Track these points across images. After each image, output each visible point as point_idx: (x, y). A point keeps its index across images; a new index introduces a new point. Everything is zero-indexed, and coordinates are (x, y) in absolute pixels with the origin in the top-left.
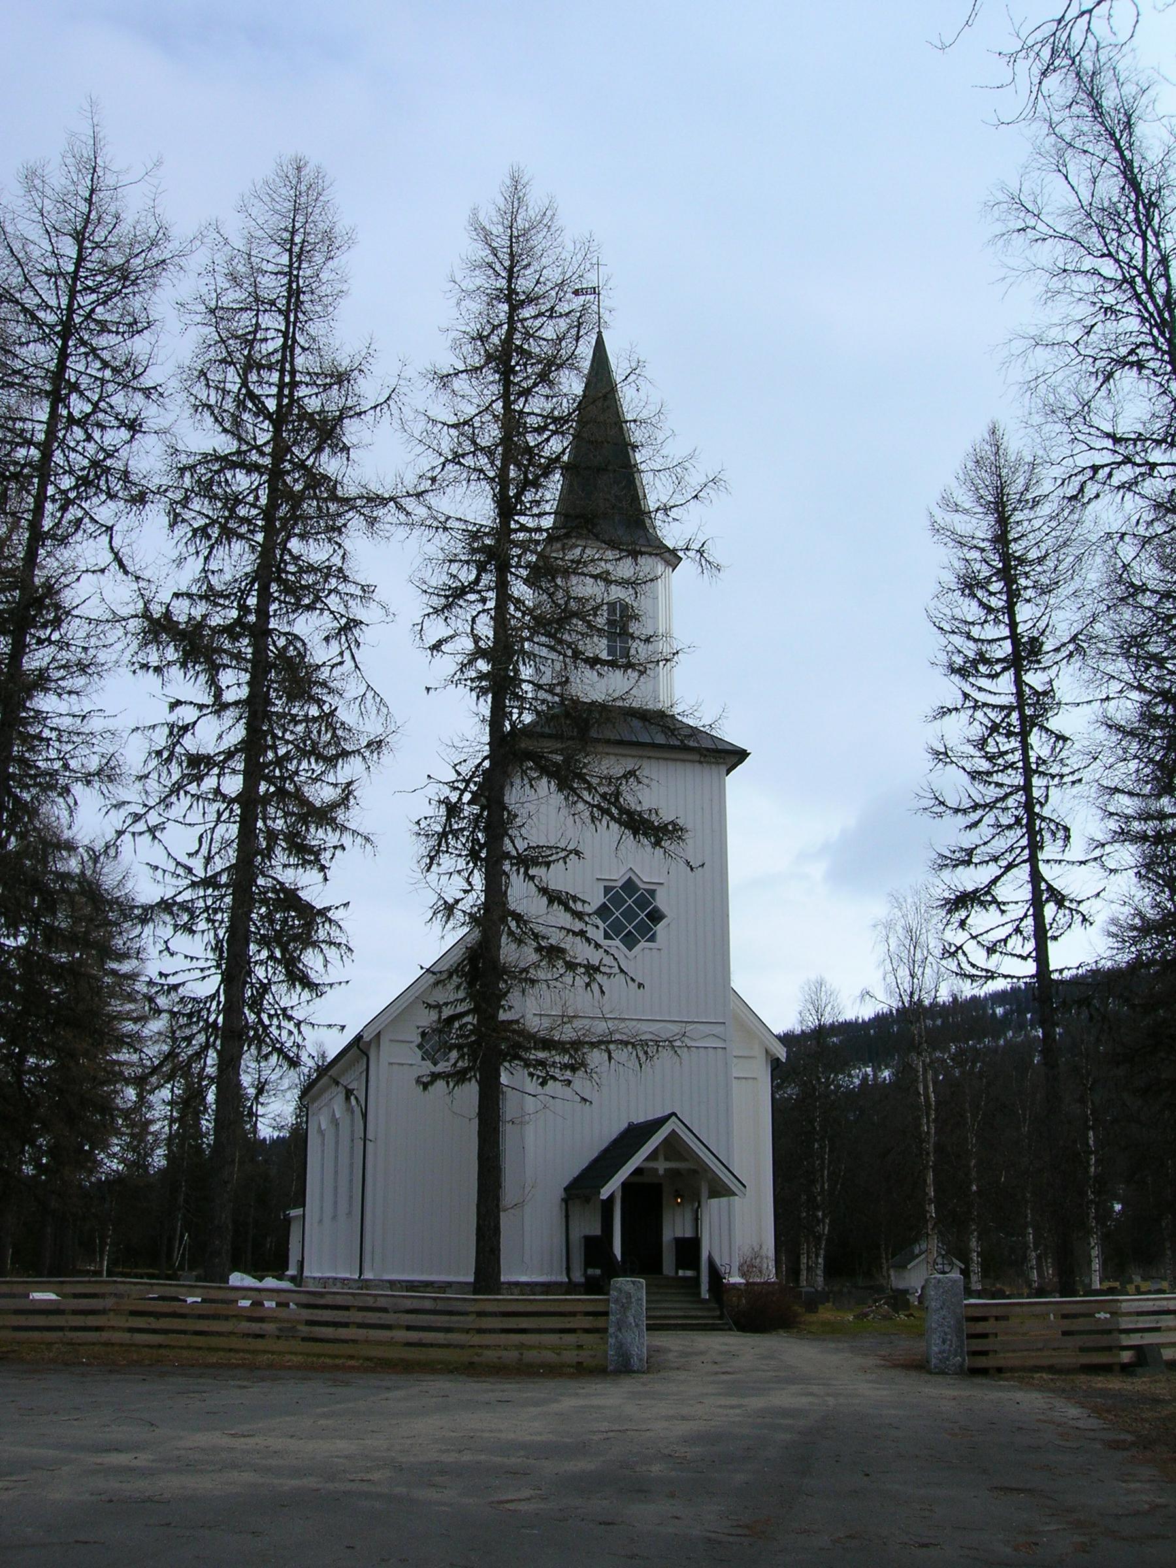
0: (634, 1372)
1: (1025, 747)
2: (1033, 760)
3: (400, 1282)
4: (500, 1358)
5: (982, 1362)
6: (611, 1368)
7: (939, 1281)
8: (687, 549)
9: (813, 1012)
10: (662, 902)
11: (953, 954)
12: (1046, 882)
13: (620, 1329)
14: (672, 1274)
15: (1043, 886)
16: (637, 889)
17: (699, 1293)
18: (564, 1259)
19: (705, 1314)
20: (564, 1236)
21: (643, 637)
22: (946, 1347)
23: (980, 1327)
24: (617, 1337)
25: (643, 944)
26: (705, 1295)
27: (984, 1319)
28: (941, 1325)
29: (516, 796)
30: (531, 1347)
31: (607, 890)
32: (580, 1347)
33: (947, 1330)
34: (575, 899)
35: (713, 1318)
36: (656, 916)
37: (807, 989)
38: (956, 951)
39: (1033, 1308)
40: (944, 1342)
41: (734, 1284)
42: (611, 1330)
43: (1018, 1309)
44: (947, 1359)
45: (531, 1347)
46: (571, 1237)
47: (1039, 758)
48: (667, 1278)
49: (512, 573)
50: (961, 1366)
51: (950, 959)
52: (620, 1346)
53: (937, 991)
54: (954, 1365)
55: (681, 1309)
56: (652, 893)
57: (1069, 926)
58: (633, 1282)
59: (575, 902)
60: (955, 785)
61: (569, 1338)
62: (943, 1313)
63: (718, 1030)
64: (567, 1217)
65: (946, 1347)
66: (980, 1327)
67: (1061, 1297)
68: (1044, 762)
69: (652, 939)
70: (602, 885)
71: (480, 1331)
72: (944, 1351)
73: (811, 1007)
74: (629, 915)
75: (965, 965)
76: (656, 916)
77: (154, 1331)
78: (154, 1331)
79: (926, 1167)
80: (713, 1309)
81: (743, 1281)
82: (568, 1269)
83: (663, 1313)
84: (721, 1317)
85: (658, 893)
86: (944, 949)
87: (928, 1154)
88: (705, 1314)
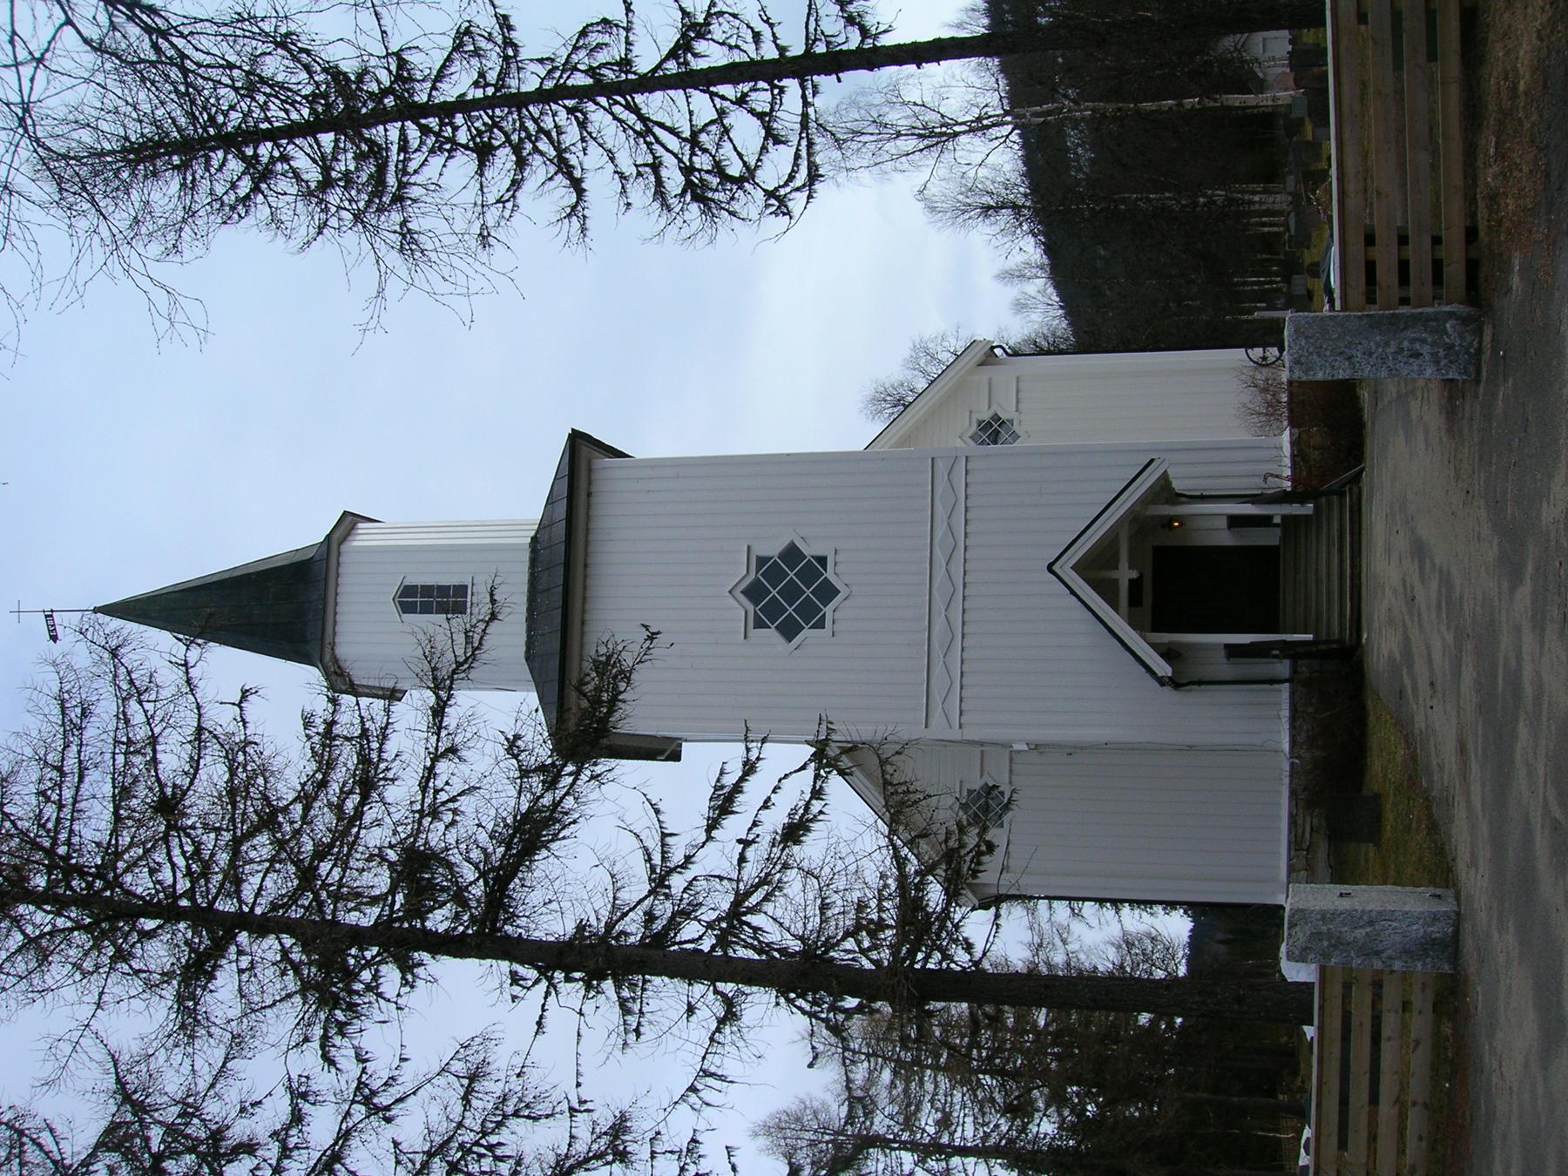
0: (1457, 933)
1: (463, 105)
2: (479, 94)
3: (1290, 859)
4: (1420, 1138)
5: (1455, 272)
6: (1447, 968)
8: (186, 664)
9: (967, 216)
10: (773, 549)
11: (782, 201)
13: (1377, 953)
14: (1278, 531)
15: (672, 66)
16: (757, 581)
17: (1306, 516)
18: (1255, 687)
21: (331, 708)
23: (1387, 275)
24: (1390, 958)
25: (829, 575)
26: (1308, 509)
27: (1370, 267)
28: (1384, 359)
29: (553, 926)
30: (1403, 1087)
31: (759, 624)
32: (1406, 1006)
33: (1392, 349)
35: (1342, 506)
36: (792, 554)
40: (1418, 355)
41: (1292, 444)
42: (1378, 965)
44: (1450, 347)
45: (1403, 1087)
46: (1228, 678)
47: (476, 84)
48: (1284, 538)
49: (252, 909)
50: (1464, 320)
56: (762, 561)
57: (735, 16)
58: (1292, 926)
59: (722, 787)
60: (543, 196)
63: (940, 464)
64: (1200, 683)
66: (1387, 275)
67: (1324, 25)
68: (482, 75)
69: (822, 560)
70: (753, 632)
71: (1373, 1138)
72: (1434, 355)
73: (960, 220)
75: (798, 182)
76: (792, 554)
79: (1138, 112)
80: (1329, 504)
81: (1287, 432)
82: (1272, 681)
83: (1335, 578)
84: (1341, 495)
85: (763, 554)
87: (1119, 109)
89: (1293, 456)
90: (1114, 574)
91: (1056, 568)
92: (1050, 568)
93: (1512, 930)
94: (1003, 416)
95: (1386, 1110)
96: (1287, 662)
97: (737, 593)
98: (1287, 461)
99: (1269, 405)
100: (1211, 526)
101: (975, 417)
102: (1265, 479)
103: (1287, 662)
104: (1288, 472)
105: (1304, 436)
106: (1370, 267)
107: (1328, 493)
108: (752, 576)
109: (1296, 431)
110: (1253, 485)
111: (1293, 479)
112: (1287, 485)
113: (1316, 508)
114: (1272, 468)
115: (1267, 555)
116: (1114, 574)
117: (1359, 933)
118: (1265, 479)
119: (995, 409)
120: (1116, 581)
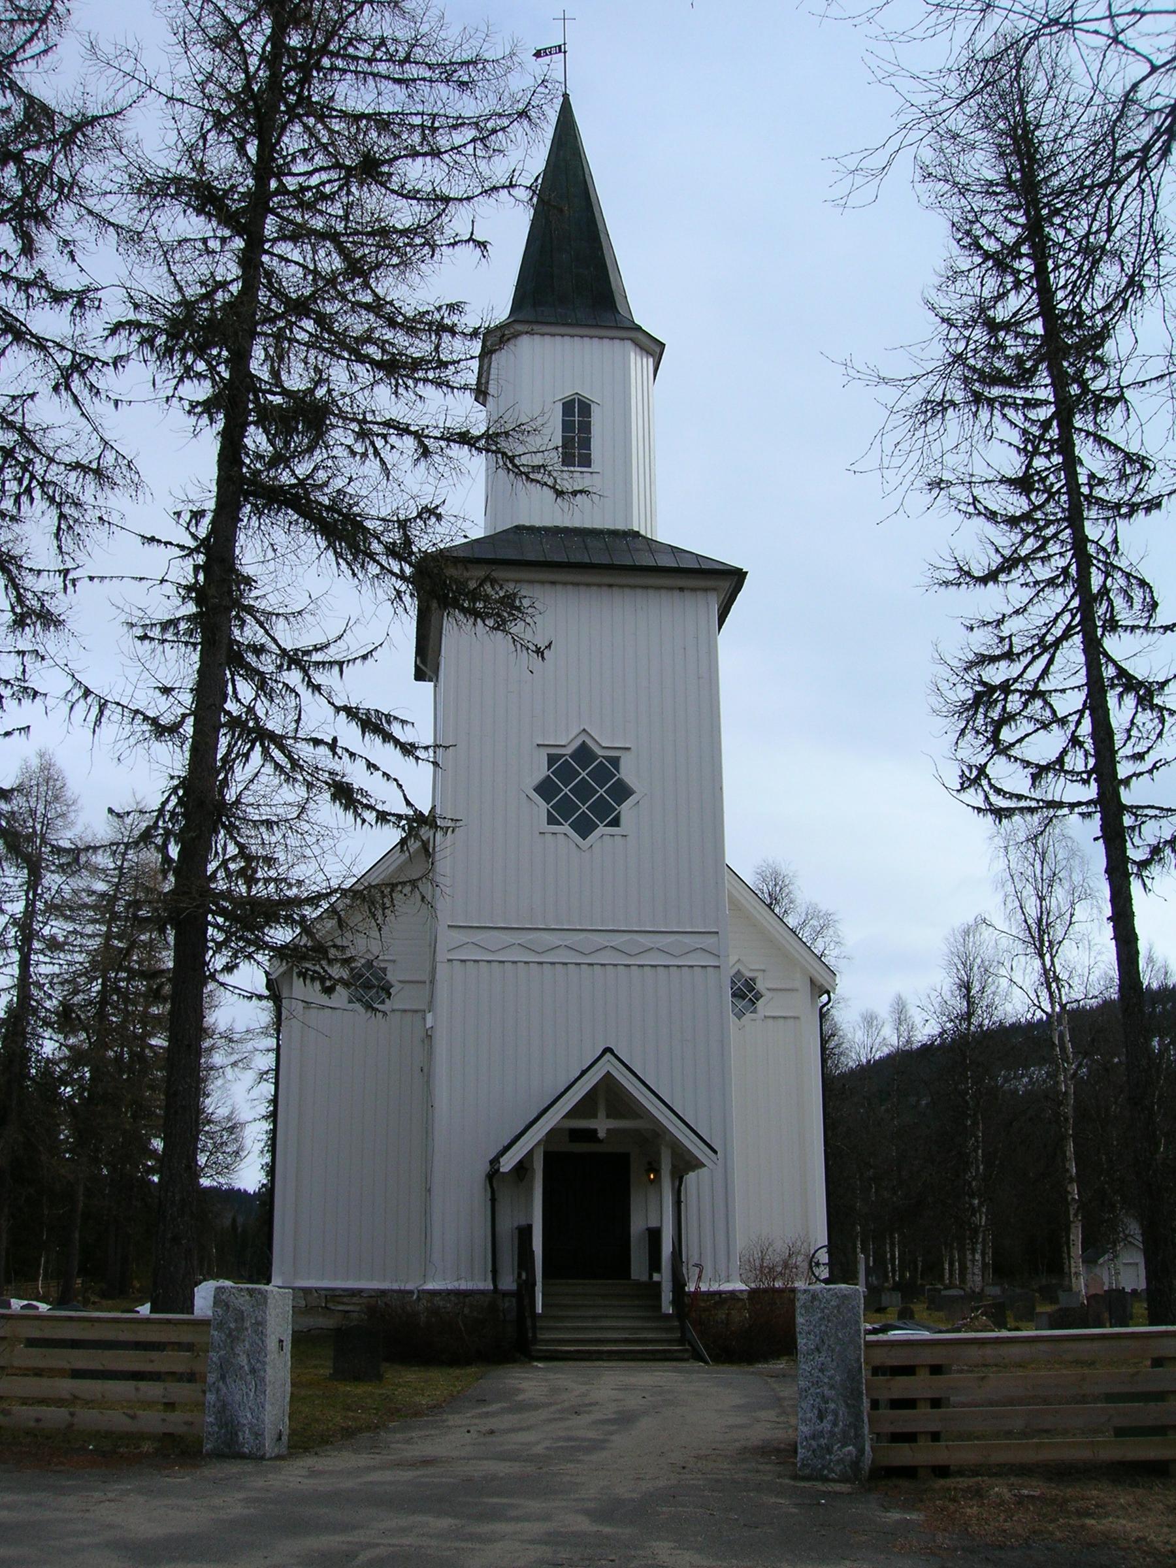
0: (243, 1457)
1: (1071, 463)
2: (1082, 479)
4: (38, 1420)
5: (904, 1455)
6: (208, 1447)
7: (814, 1297)
8: (512, 186)
9: (960, 967)
10: (628, 773)
11: (975, 782)
12: (1115, 663)
13: (223, 1377)
15: (1109, 672)
17: (660, 1307)
19: (664, 1336)
20: (489, 1224)
21: (468, 331)
22: (826, 1425)
23: (901, 1387)
24: (218, 1390)
25: (602, 829)
27: (909, 1370)
28: (817, 1384)
30: (88, 1403)
31: (552, 759)
32: (170, 1406)
33: (827, 1392)
34: (389, 718)
35: (670, 1342)
37: (952, 940)
38: (978, 777)
39: (1004, 1350)
40: (821, 1417)
41: (732, 1292)
43: (974, 1353)
45: (88, 1403)
47: (1092, 476)
48: (638, 1284)
49: (267, 252)
50: (856, 1464)
51: (972, 790)
52: (223, 1407)
53: (1072, 915)
54: (840, 1461)
55: (624, 1329)
56: (615, 762)
57: (1160, 735)
58: (251, 1292)
59: (389, 722)
61: (152, 1390)
62: (821, 1358)
63: (709, 941)
64: (493, 1200)
65: (826, 1425)
66: (901, 1387)
68: (1101, 482)
69: (616, 822)
72: (821, 1434)
73: (956, 960)
74: (583, 791)
76: (622, 792)
77: (601, 1328)
78: (601, 1328)
82: (495, 1272)
84: (681, 1341)
86: (963, 775)
87: (1066, 1119)
88: (664, 1336)
89: (719, 1293)
90: (602, 1113)
91: (608, 1056)
92: (608, 1050)
93: (246, 1511)
94: (760, 1003)
95: (66, 1386)
96: (514, 1287)
97: (583, 738)
98: (715, 1287)
99: (772, 1269)
100: (651, 1211)
101: (760, 977)
102: (696, 1265)
103: (514, 1287)
104: (704, 1288)
105: (740, 1304)
106: (909, 1370)
107: (683, 1329)
108: (600, 752)
109: (745, 1296)
110: (691, 1253)
111: (697, 1293)
112: (691, 1287)
113: (668, 1316)
114: (708, 1271)
115: (622, 1268)
116: (602, 1113)
117: (243, 1360)
118: (696, 1265)
119: (768, 995)
120: (595, 1116)
